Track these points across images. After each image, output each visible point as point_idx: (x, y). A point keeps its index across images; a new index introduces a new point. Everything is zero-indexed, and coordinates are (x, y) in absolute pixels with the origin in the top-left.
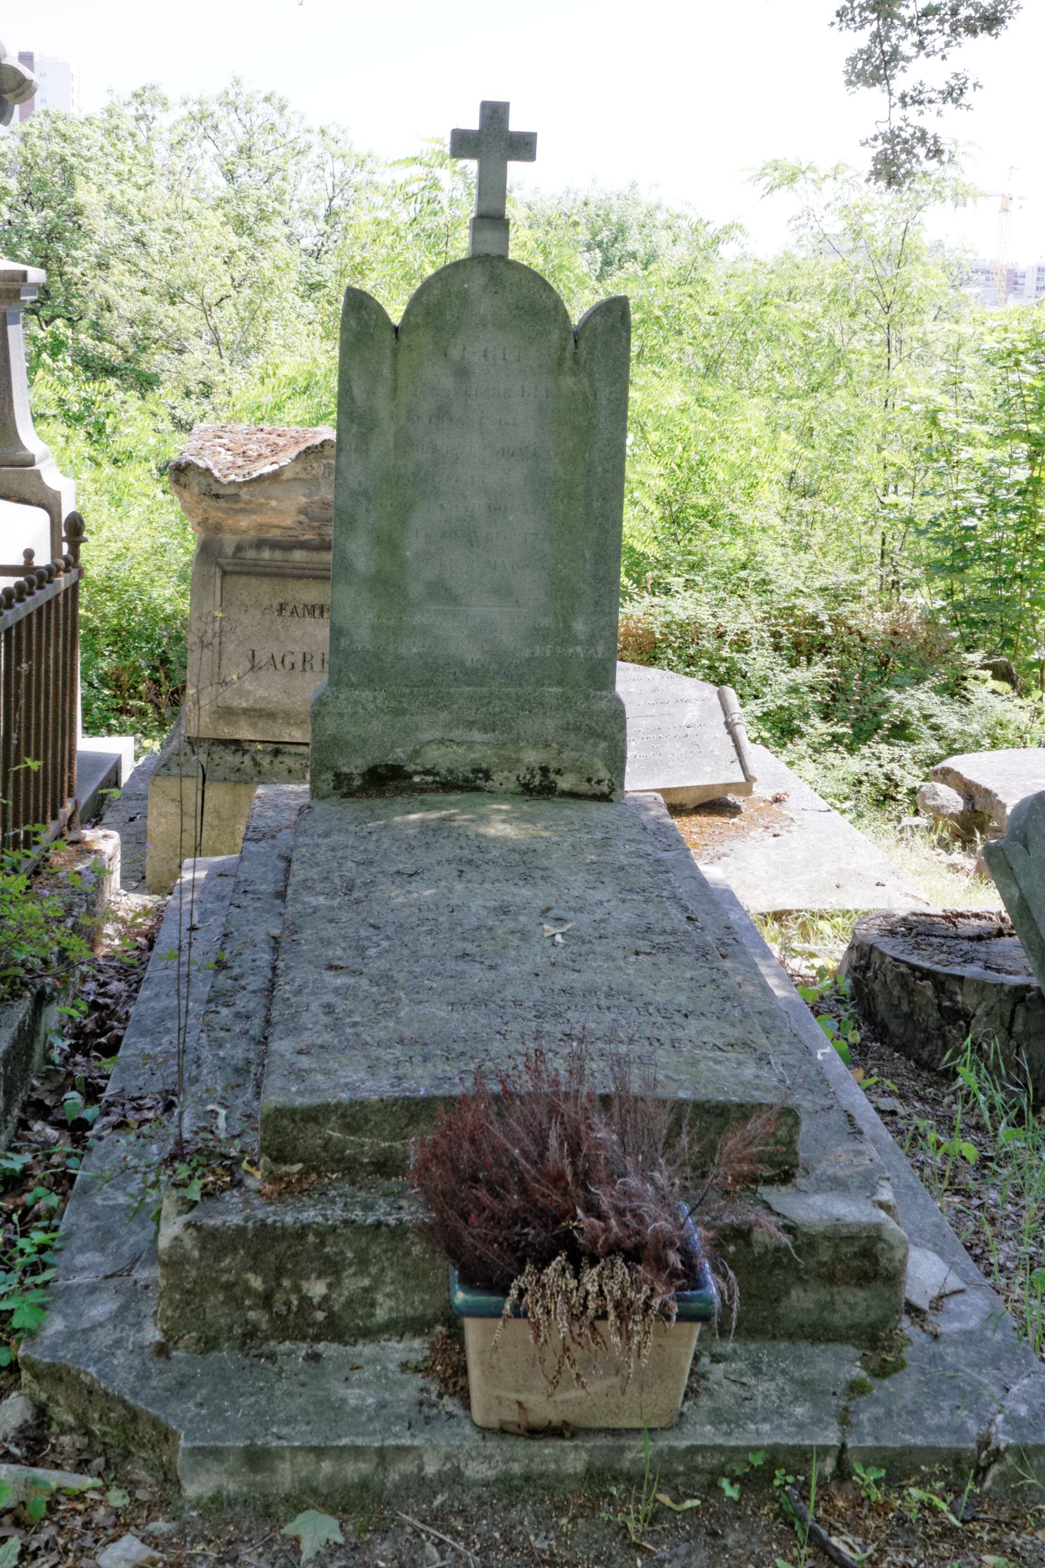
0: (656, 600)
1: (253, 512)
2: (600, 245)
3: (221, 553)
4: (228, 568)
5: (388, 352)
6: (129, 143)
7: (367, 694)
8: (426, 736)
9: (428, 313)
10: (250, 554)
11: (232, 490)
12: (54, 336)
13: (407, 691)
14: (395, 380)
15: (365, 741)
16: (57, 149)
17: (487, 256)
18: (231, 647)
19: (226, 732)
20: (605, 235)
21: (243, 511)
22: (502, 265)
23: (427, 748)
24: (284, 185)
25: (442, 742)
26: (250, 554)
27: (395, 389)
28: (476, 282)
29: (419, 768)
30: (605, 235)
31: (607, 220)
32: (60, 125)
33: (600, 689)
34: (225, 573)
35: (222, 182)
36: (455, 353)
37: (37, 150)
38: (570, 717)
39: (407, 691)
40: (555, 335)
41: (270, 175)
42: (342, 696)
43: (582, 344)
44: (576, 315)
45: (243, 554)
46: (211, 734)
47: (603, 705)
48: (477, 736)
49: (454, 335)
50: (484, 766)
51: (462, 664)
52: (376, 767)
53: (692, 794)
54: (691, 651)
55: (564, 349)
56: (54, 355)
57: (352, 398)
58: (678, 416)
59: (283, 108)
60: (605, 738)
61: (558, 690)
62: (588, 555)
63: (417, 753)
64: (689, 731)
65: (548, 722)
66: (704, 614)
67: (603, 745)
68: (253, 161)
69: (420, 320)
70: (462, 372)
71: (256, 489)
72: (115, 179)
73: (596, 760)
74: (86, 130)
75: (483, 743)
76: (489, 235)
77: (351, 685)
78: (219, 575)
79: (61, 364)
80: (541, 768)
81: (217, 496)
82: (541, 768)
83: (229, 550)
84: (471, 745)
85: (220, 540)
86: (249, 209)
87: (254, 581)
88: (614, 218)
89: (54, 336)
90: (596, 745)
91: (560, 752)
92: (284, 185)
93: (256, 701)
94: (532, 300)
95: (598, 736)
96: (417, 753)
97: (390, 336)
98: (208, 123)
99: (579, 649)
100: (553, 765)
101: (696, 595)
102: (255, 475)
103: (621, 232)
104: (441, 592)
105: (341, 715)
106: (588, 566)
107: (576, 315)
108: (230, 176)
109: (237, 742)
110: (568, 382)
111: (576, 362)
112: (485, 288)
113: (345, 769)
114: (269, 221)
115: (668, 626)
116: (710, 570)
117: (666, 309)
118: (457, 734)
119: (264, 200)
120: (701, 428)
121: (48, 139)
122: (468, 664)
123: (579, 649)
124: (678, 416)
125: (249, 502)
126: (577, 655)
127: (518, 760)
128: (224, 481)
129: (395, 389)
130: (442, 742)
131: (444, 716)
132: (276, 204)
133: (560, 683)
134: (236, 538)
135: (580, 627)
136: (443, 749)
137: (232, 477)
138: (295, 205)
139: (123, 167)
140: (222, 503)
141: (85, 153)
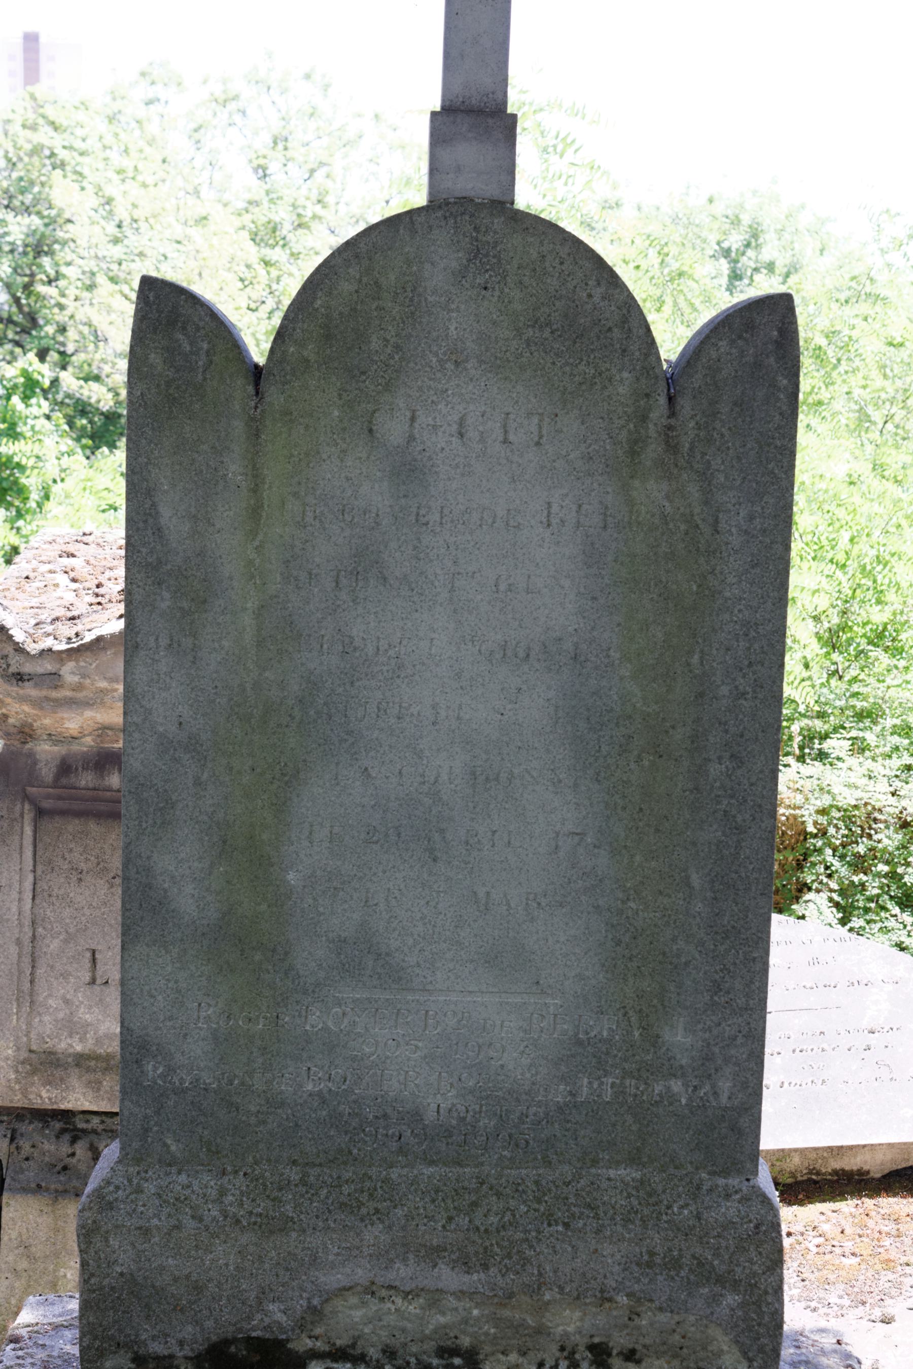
0: (806, 770)
1: (87, 704)
2: (727, 253)
3: (32, 777)
4: (46, 804)
5: (239, 426)
6: (137, 133)
7: (208, 1182)
8: (333, 1279)
9: (328, 337)
10: (86, 779)
11: (48, 666)
12: (25, 373)
13: (294, 1174)
14: (255, 490)
15: (198, 1288)
16: (47, 142)
17: (464, 201)
18: (54, 945)
19: (45, 1096)
20: (735, 241)
21: (71, 703)
22: (498, 223)
23: (338, 1303)
24: (329, 184)
25: (370, 1290)
26: (86, 779)
27: (255, 512)
28: (442, 261)
29: (320, 1345)
30: (735, 241)
31: (736, 222)
32: (50, 111)
33: (725, 1173)
34: (40, 813)
35: (252, 179)
36: (393, 429)
37: (21, 142)
38: (656, 1239)
39: (294, 1174)
40: (624, 385)
41: (312, 171)
42: (150, 1188)
43: (685, 405)
44: (671, 340)
45: (72, 779)
46: (18, 1101)
47: (730, 1209)
48: (448, 1277)
49: (388, 387)
50: (466, 1342)
51: (416, 1116)
52: (227, 1342)
53: (879, 1157)
54: (861, 849)
55: (644, 418)
56: (26, 398)
57: (159, 531)
58: (845, 492)
59: (326, 87)
60: (735, 1285)
61: (629, 1174)
62: (696, 880)
63: (315, 1313)
64: (873, 1040)
65: (607, 1249)
66: (878, 794)
67: (732, 1299)
68: (289, 154)
69: (310, 351)
70: (408, 470)
71: (89, 663)
72: (116, 178)
73: (715, 1332)
74: (81, 116)
75: (461, 1294)
76: (470, 153)
77: (169, 1163)
78: (28, 818)
79: (35, 410)
80: (592, 1348)
81: (20, 678)
82: (592, 1348)
83: (47, 773)
84: (435, 1298)
85: (31, 755)
86: (283, 215)
87: (92, 826)
88: (746, 219)
89: (25, 373)
90: (715, 1299)
91: (634, 1314)
92: (329, 184)
93: (98, 1041)
94: (569, 297)
95: (720, 1280)
96: (315, 1313)
97: (242, 388)
98: (232, 106)
99: (676, 1086)
100: (620, 1341)
101: (869, 764)
102: (88, 637)
103: (753, 240)
104: (365, 959)
105: (145, 1232)
106: (698, 906)
107: (671, 340)
108: (263, 173)
109: (66, 1115)
110: (652, 492)
111: (672, 447)
112: (461, 274)
113: (157, 1348)
114: (308, 228)
115: (823, 812)
116: (889, 722)
117: (830, 335)
118: (403, 1272)
119: (301, 201)
120: (876, 508)
121: (34, 128)
122: (430, 1115)
123: (676, 1086)
124: (845, 492)
125: (79, 687)
126: (673, 1099)
127: (540, 1331)
128: (33, 648)
129: (255, 512)
130: (370, 1290)
131: (374, 1234)
132: (318, 209)
133: (634, 1160)
134: (59, 750)
135: (679, 1037)
136: (374, 1306)
137: (49, 643)
138: (342, 208)
139: (128, 163)
140: (30, 690)
141: (78, 144)
